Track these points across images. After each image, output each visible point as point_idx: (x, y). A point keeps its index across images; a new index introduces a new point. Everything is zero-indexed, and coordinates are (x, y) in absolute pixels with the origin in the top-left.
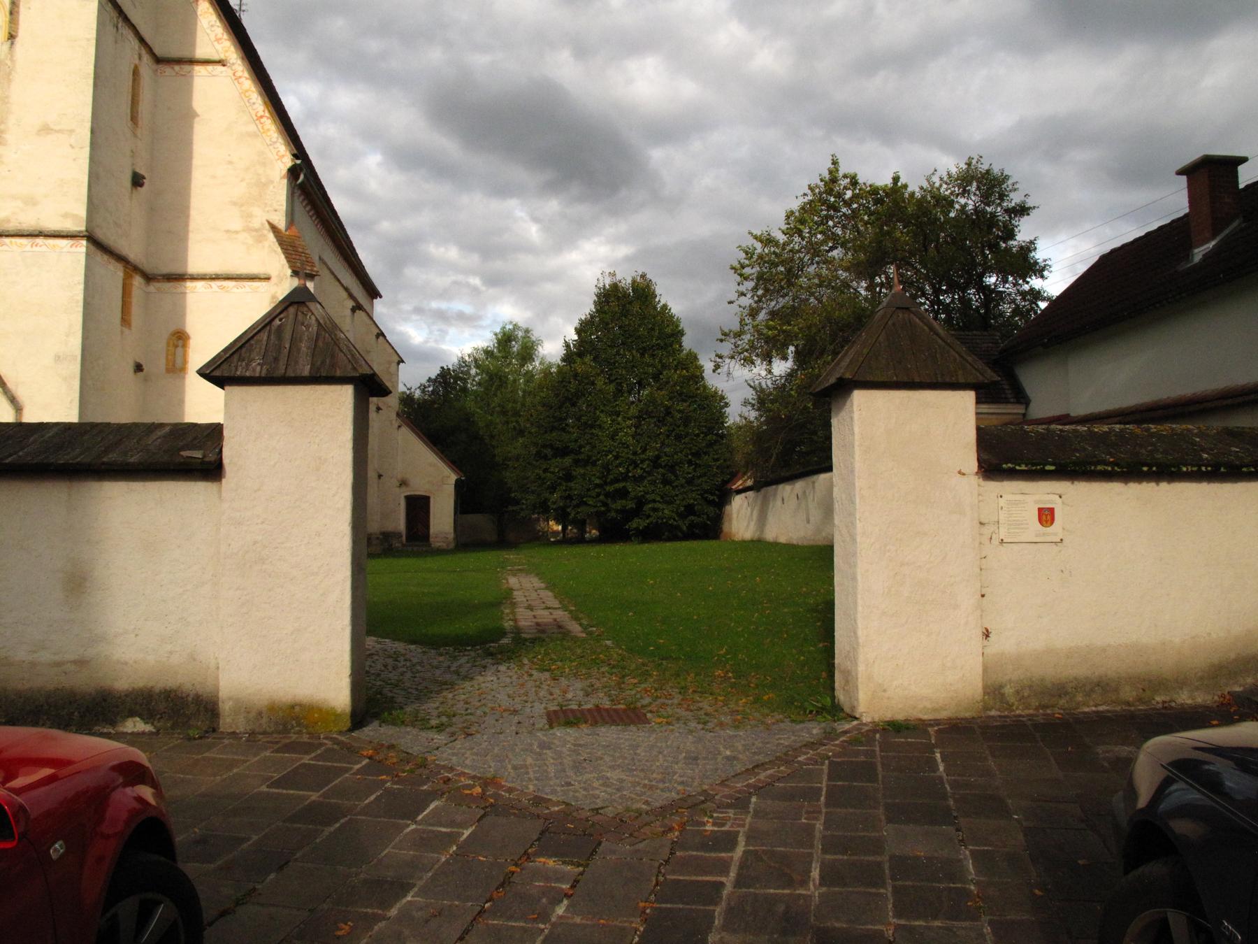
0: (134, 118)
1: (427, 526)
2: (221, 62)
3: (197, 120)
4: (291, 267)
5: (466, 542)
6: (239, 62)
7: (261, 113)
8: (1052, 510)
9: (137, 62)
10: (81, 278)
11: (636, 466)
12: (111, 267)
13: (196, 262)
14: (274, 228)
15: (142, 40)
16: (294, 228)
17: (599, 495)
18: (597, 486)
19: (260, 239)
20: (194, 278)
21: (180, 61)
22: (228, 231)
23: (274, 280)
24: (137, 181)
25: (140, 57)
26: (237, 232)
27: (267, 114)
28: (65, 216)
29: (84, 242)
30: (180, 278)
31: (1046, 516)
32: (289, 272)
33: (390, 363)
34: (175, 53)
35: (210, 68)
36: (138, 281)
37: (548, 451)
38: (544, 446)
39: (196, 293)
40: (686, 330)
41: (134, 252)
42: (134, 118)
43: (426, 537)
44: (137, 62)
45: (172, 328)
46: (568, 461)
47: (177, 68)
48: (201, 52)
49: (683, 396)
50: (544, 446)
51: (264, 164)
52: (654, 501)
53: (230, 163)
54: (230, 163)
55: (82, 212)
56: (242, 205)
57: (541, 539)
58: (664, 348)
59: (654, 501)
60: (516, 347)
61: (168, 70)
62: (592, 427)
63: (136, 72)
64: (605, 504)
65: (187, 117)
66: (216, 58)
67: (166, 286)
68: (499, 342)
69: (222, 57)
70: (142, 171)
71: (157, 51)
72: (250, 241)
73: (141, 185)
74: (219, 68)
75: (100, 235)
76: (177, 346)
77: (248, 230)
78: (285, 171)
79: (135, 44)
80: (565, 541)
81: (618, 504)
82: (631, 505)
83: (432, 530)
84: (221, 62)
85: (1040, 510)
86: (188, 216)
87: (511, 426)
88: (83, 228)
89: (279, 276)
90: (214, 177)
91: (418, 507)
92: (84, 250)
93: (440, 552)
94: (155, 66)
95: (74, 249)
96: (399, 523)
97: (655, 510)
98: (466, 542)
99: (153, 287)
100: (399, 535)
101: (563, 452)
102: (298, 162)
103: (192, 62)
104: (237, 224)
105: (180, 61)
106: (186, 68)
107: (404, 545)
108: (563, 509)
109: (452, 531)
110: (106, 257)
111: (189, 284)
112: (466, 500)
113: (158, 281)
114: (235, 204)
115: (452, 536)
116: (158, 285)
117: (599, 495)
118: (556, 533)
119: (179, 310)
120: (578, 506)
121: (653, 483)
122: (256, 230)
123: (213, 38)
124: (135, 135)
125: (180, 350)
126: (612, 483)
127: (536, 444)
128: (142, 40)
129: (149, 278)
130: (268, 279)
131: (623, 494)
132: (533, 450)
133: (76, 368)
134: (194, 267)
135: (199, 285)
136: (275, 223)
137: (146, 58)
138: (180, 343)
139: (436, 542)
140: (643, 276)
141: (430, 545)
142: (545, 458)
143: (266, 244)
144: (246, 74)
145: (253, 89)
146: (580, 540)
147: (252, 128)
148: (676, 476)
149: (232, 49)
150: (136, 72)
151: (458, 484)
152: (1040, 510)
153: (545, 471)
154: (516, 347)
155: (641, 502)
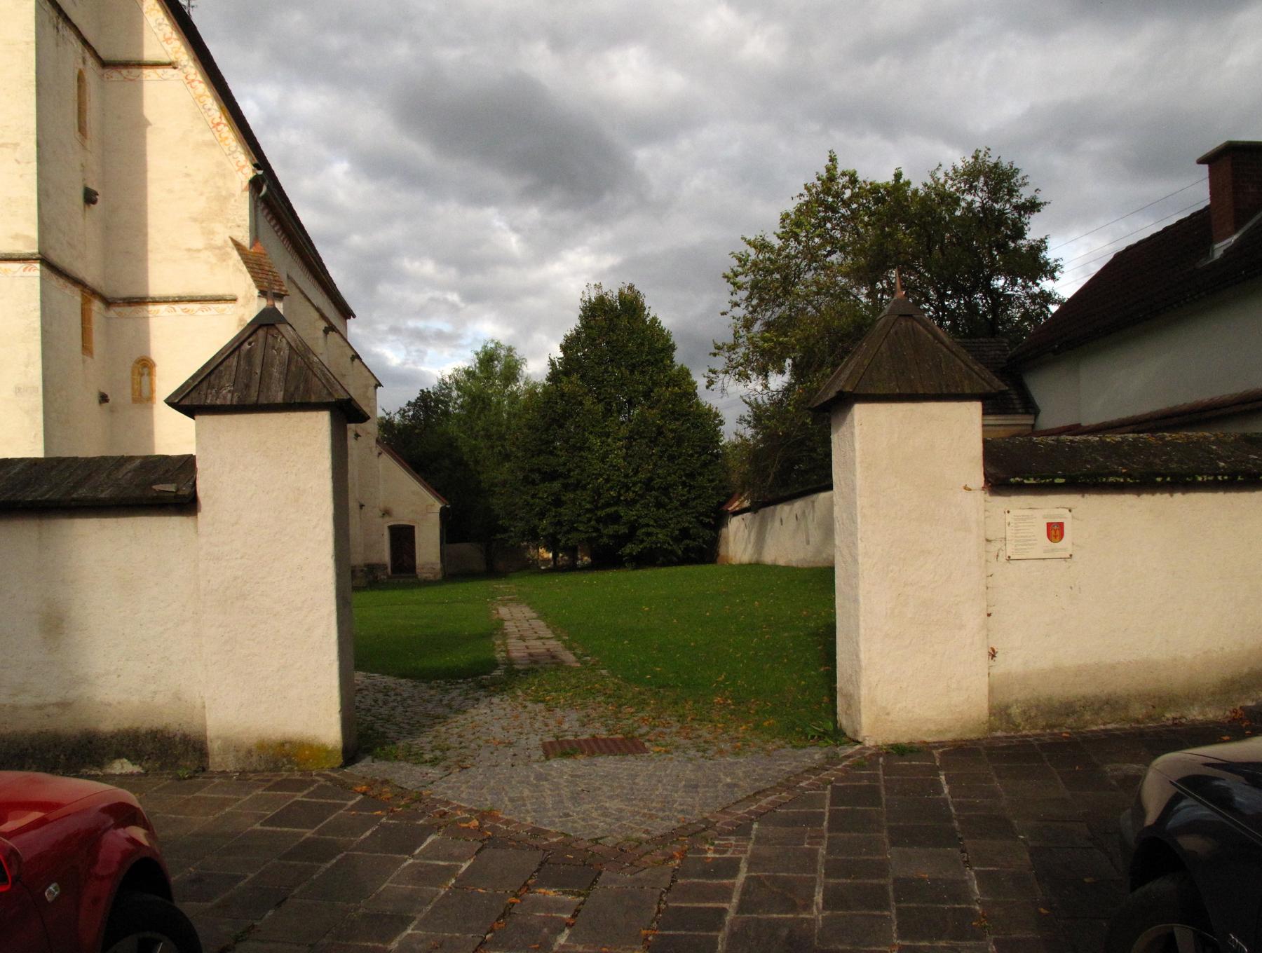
0: (82, 129)
1: (413, 557)
2: (172, 65)
3: (149, 129)
4: (257, 287)
5: (453, 572)
6: (191, 64)
7: (217, 120)
8: (1061, 525)
9: (81, 66)
10: (37, 304)
11: (628, 489)
12: (68, 291)
13: (157, 285)
14: (237, 245)
15: (85, 42)
16: (259, 245)
17: (589, 520)
18: (588, 511)
19: (224, 258)
20: (156, 301)
21: (127, 65)
22: (189, 250)
23: (240, 301)
24: (90, 197)
25: (84, 61)
26: (199, 251)
27: (224, 121)
28: (16, 237)
29: (38, 266)
30: (142, 301)
31: (1055, 531)
32: (256, 292)
33: (367, 387)
34: (121, 56)
35: (160, 71)
36: (97, 306)
37: (536, 476)
38: (532, 471)
39: (159, 316)
40: (677, 345)
41: (91, 275)
42: (82, 129)
43: (412, 568)
44: (81, 66)
45: (136, 356)
46: (557, 485)
47: (124, 72)
48: (149, 54)
49: (675, 415)
50: (532, 471)
51: (224, 176)
52: (648, 525)
53: (188, 175)
54: (188, 175)
55: (34, 233)
56: (203, 221)
57: (531, 567)
58: (655, 363)
59: (648, 525)
60: (498, 367)
61: (115, 74)
62: (581, 449)
63: (81, 78)
64: (597, 530)
65: (140, 125)
66: (166, 59)
67: (128, 310)
68: (481, 362)
69: (173, 58)
70: (94, 187)
71: (103, 54)
72: (213, 260)
73: (94, 202)
74: (170, 71)
75: (54, 257)
76: (142, 375)
77: (211, 247)
78: (246, 183)
79: (78, 46)
80: (556, 569)
81: (610, 530)
82: (623, 530)
83: (419, 561)
84: (172, 65)
85: (1049, 525)
86: (146, 235)
87: (496, 450)
88: (36, 251)
89: (245, 297)
90: (171, 191)
91: (403, 537)
92: (38, 273)
93: (427, 583)
94: (101, 71)
95: (27, 273)
96: (384, 554)
97: (649, 534)
98: (453, 572)
99: (113, 312)
100: (384, 567)
101: (551, 476)
102: (260, 172)
103: (141, 65)
104: (198, 243)
105: (127, 65)
106: (135, 71)
107: (389, 577)
108: (553, 536)
109: (439, 561)
110: (62, 281)
111: (152, 308)
112: (452, 529)
113: (119, 305)
114: (195, 220)
115: (438, 566)
116: (118, 309)
117: (589, 520)
118: (546, 561)
119: (143, 336)
120: (568, 532)
121: (646, 506)
122: (219, 248)
123: (161, 37)
124: (84, 147)
125: (145, 378)
126: (603, 507)
127: (522, 469)
128: (85, 42)
129: (108, 302)
130: (234, 300)
131: (615, 518)
132: (520, 475)
133: (38, 400)
134: (155, 290)
135: (162, 308)
136: (239, 239)
137: (91, 62)
138: (146, 371)
139: (422, 573)
140: (631, 288)
141: (416, 576)
142: (533, 483)
143: (231, 263)
144: (199, 78)
145: (208, 93)
146: (572, 568)
147: (209, 136)
148: (670, 499)
149: (183, 49)
150: (81, 78)
151: (444, 514)
152: (1049, 525)
153: (534, 496)
154: (498, 367)
155: (633, 527)
